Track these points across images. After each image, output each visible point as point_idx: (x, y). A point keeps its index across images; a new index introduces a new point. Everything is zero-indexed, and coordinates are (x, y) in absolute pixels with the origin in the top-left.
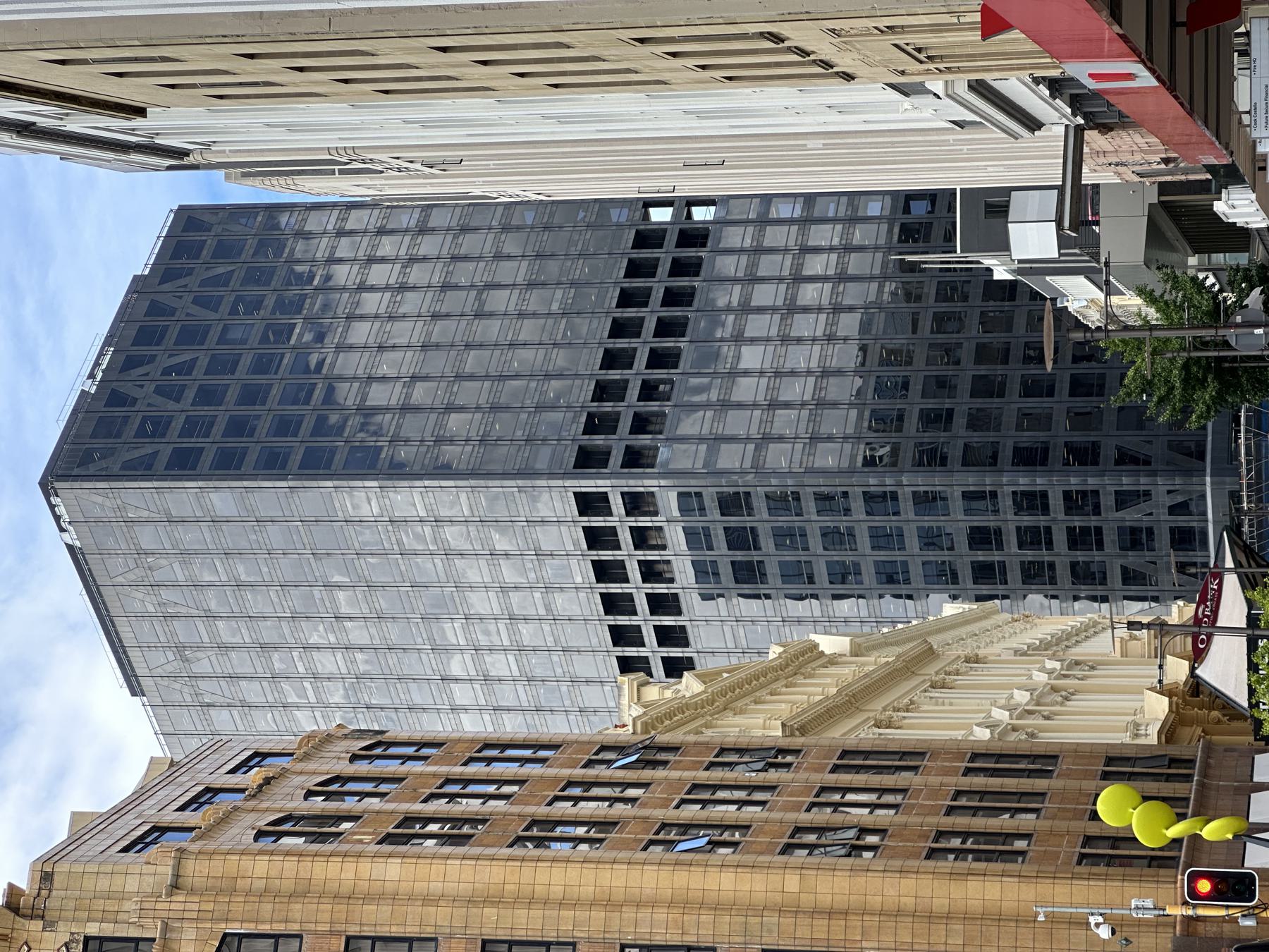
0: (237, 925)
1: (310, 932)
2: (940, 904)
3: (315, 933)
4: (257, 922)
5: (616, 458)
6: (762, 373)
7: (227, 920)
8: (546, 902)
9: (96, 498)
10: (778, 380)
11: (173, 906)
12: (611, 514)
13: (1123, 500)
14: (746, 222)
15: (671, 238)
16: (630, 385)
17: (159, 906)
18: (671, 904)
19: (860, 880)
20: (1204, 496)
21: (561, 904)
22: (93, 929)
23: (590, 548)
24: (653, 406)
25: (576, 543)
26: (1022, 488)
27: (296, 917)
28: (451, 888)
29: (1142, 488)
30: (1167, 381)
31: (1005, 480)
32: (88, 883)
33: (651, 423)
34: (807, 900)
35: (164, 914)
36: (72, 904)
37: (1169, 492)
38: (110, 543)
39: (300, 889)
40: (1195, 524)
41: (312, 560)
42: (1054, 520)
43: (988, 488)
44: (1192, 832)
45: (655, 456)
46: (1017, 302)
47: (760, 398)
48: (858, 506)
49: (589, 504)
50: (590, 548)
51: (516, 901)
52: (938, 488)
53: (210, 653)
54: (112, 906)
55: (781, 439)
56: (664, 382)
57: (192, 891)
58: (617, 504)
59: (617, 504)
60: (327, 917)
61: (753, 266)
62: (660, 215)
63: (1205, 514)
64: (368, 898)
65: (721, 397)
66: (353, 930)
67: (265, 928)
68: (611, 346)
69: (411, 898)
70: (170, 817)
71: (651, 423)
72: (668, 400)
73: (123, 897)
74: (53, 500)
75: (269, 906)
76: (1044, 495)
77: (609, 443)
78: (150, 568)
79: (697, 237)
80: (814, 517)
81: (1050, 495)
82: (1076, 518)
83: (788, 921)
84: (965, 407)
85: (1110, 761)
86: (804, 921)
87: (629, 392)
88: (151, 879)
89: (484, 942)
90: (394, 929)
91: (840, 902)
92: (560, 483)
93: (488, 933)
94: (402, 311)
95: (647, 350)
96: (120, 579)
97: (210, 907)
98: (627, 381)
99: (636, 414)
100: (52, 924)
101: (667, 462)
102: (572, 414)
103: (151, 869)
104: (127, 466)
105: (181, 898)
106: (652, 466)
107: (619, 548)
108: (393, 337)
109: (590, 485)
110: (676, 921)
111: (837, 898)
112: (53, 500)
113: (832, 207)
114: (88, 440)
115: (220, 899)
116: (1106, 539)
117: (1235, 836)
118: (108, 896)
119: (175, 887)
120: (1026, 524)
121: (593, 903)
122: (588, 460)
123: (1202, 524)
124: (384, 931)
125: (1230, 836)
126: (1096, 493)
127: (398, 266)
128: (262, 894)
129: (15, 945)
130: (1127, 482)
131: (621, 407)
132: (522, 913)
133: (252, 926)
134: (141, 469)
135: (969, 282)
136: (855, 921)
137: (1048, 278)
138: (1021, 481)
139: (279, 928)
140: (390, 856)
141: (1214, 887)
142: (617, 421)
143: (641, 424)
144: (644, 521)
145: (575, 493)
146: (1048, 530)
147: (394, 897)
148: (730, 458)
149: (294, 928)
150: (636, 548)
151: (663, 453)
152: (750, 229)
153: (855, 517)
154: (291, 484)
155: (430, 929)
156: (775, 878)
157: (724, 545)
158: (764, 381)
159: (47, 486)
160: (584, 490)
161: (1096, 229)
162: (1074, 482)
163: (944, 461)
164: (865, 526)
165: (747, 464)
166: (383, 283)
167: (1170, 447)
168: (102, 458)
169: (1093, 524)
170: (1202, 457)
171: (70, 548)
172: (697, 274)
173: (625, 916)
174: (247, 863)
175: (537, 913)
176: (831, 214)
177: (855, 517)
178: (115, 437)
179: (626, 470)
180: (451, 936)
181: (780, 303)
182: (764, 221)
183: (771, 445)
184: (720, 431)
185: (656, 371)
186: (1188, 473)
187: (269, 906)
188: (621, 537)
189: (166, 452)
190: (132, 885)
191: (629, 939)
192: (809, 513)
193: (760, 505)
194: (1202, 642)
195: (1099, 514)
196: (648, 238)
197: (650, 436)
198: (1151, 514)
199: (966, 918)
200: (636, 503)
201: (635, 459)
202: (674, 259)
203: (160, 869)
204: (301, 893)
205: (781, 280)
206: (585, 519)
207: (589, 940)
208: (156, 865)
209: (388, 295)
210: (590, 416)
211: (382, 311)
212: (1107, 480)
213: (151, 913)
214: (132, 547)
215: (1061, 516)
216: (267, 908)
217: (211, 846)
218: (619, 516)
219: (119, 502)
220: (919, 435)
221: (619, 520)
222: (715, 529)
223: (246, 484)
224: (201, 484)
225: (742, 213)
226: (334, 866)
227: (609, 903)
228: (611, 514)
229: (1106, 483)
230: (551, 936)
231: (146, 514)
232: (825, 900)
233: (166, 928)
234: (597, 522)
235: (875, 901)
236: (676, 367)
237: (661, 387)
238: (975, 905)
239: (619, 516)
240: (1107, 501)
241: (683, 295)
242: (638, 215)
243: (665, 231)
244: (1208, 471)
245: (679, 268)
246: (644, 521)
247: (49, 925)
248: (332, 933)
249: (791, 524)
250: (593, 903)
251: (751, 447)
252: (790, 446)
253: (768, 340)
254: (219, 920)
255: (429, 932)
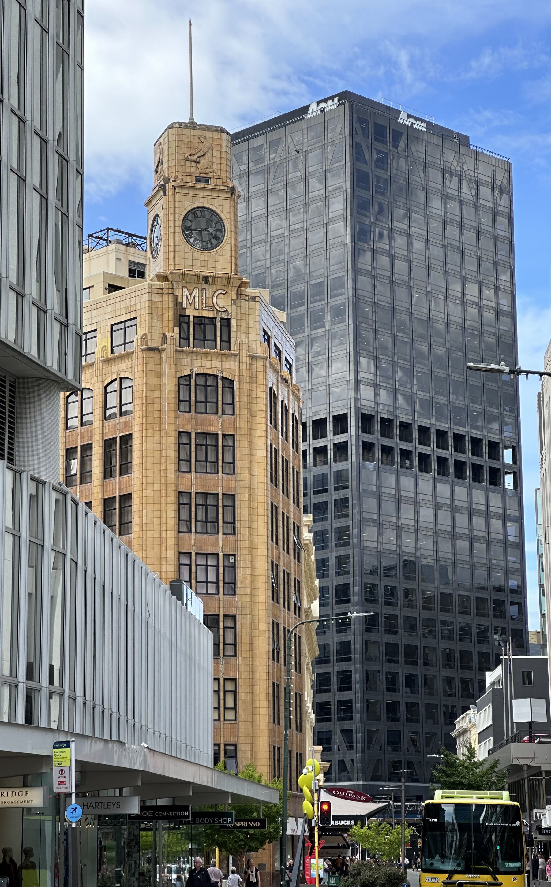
0: (238, 386)
1: (236, 418)
2: (257, 689)
3: (235, 421)
4: (239, 395)
5: (367, 438)
6: (417, 521)
7: (240, 382)
8: (251, 521)
9: (339, 132)
10: (413, 531)
11: (245, 358)
12: (334, 434)
13: (347, 733)
14: (504, 509)
15: (495, 464)
16: (409, 444)
17: (245, 351)
18: (252, 575)
19: (265, 656)
20: (350, 780)
21: (250, 528)
22: (233, 322)
23: (314, 421)
24: (397, 458)
25: (316, 413)
26: (353, 676)
27: (242, 412)
28: (255, 479)
29: (354, 745)
30: (453, 774)
31: (358, 666)
32: (251, 318)
33: (387, 456)
34: (256, 633)
35: (241, 354)
36: (243, 311)
37: (352, 760)
38: (311, 134)
39: (253, 412)
40: (333, 775)
41: (303, 255)
42: (334, 694)
43: (353, 656)
44: (306, 797)
45: (368, 461)
46: (460, 671)
47: (403, 521)
48: (342, 580)
49: (341, 422)
50: (314, 421)
51: (251, 508)
52: (352, 627)
53: (245, 191)
54: (243, 329)
55: (380, 534)
56: (411, 463)
57: (251, 365)
58: (341, 438)
59: (341, 438)
60: (242, 426)
61: (479, 512)
62: (508, 456)
63: (340, 781)
64: (250, 443)
65: (403, 498)
66: (237, 438)
67: (237, 399)
68: (432, 431)
69: (251, 462)
70: (273, 341)
71: (387, 456)
72: (401, 467)
73: (247, 334)
74: (336, 100)
75: (246, 400)
76: (350, 689)
77: (376, 433)
78: (297, 158)
79: (495, 479)
80: (334, 554)
81: (349, 692)
82: (336, 707)
83: (248, 625)
84: (399, 642)
85: (301, 755)
86: (248, 632)
87: (405, 443)
88: (254, 345)
89: (234, 495)
90: (238, 455)
91: (256, 647)
92: (353, 405)
93: (237, 497)
94: (450, 304)
95: (429, 453)
96: (290, 140)
97: (245, 374)
98: (411, 442)
99: (393, 448)
100: (235, 304)
101: (365, 467)
102: (392, 410)
103: (258, 345)
104: (358, 145)
105: (248, 361)
106: (363, 459)
107: (314, 439)
108: (435, 300)
109: (352, 422)
110: (246, 578)
111: (257, 646)
112: (336, 100)
113: (513, 559)
114: (373, 121)
115: (248, 378)
116: (324, 724)
117: (306, 814)
118: (247, 327)
119: (253, 358)
120: (332, 678)
121: (251, 542)
122: (366, 421)
123: (334, 779)
124: (237, 451)
125: (305, 812)
126: (351, 718)
127: (476, 300)
128: (250, 396)
129: (225, 288)
130: (358, 736)
131: (397, 439)
132: (246, 511)
133: (238, 393)
134: (357, 154)
135: (471, 642)
136: (249, 654)
137: (490, 705)
138: (358, 676)
139: (237, 405)
140: (267, 451)
141: (326, 811)
142: (388, 437)
143: (387, 451)
144: (330, 454)
145: (347, 413)
146: (329, 691)
147: (251, 455)
148: (370, 504)
149: (237, 412)
150: (314, 449)
151: (370, 465)
152: (500, 511)
153: (335, 578)
154: (349, 245)
155: (239, 471)
156: (264, 619)
157: (317, 501)
158: (413, 523)
159: (343, 96)
160: (349, 419)
161: (526, 738)
162: (357, 706)
163: (368, 630)
164: (329, 584)
165: (365, 515)
166: (467, 292)
167: (378, 761)
168: (363, 129)
169: (332, 716)
170: (372, 779)
171: (305, 109)
172: (474, 480)
173: (247, 556)
174: (262, 388)
175: (247, 518)
176: (510, 558)
177: (335, 578)
178: (375, 137)
179: (361, 444)
180: (236, 480)
181: (458, 530)
182: (505, 518)
183: (376, 529)
184: (383, 498)
185: (417, 458)
186: (364, 771)
187: (246, 400)
188: (321, 440)
189: (365, 168)
190: (252, 337)
191: (238, 558)
192: (337, 551)
193: (341, 523)
194: (336, 792)
195: (339, 720)
196: (495, 449)
197: (380, 457)
198: (339, 750)
199: (252, 700)
200: (341, 449)
201: (367, 448)
202: (482, 466)
203: (258, 349)
204: (252, 413)
205: (471, 530)
206: (331, 419)
207: (236, 541)
208: (260, 349)
209: (459, 295)
210: (391, 421)
211: (450, 292)
212: (359, 725)
213: (241, 348)
214: (310, 148)
215: (337, 698)
216: (245, 399)
217: (268, 370)
218: (333, 439)
219: (337, 141)
220: (383, 615)
221: (331, 439)
222: (326, 496)
223: (349, 217)
224: (349, 191)
225: (510, 506)
226: (262, 426)
227: (252, 549)
228: (334, 434)
229: (356, 724)
230: (237, 524)
231: (330, 157)
232: (256, 641)
233: (236, 355)
234: (330, 426)
235: (257, 662)
236: (420, 470)
237: (407, 462)
238: (257, 704)
239: (333, 439)
240: (347, 725)
241: (461, 472)
242: (508, 443)
243: (499, 460)
244: (365, 783)
245: (477, 469)
246: (330, 454)
247: (234, 302)
248: (236, 428)
249: (330, 540)
250: (251, 542)
251: (375, 517)
252: (376, 539)
253: (436, 524)
254: (240, 379)
255: (238, 471)
